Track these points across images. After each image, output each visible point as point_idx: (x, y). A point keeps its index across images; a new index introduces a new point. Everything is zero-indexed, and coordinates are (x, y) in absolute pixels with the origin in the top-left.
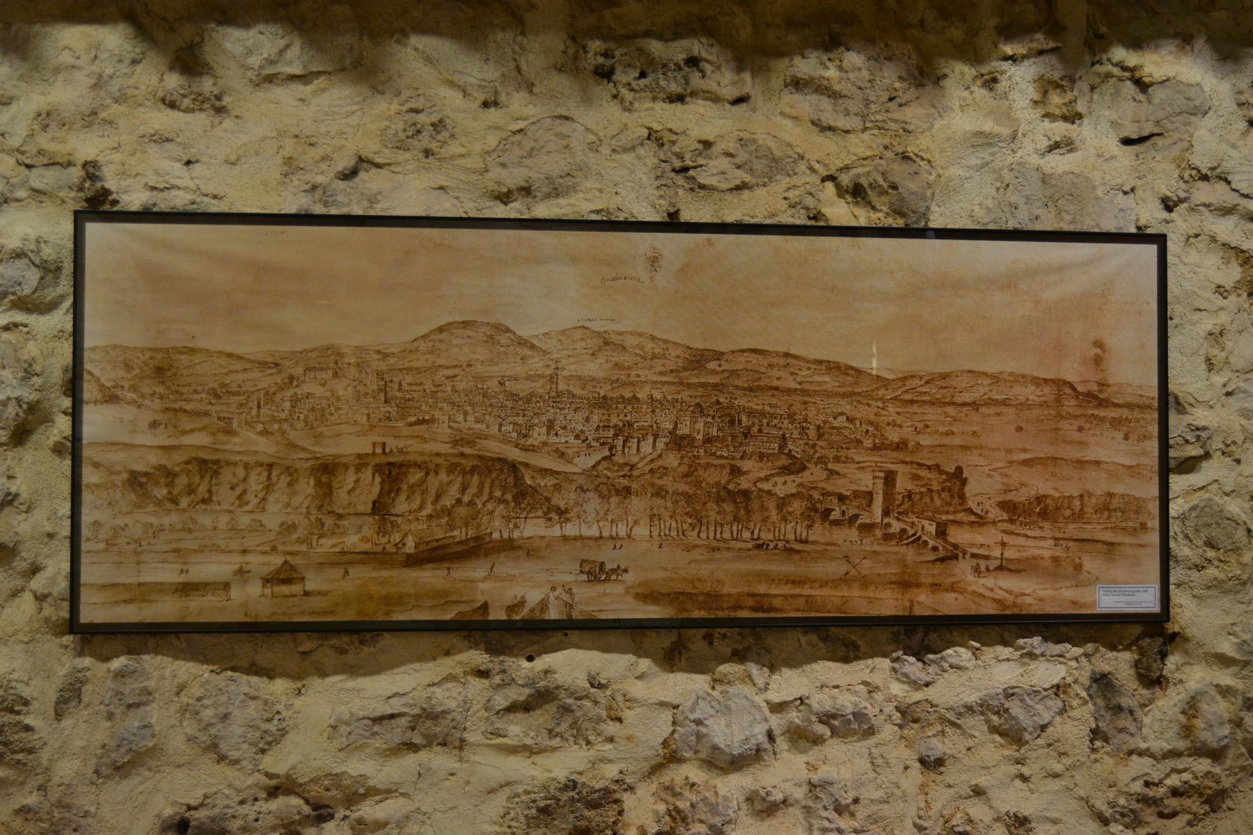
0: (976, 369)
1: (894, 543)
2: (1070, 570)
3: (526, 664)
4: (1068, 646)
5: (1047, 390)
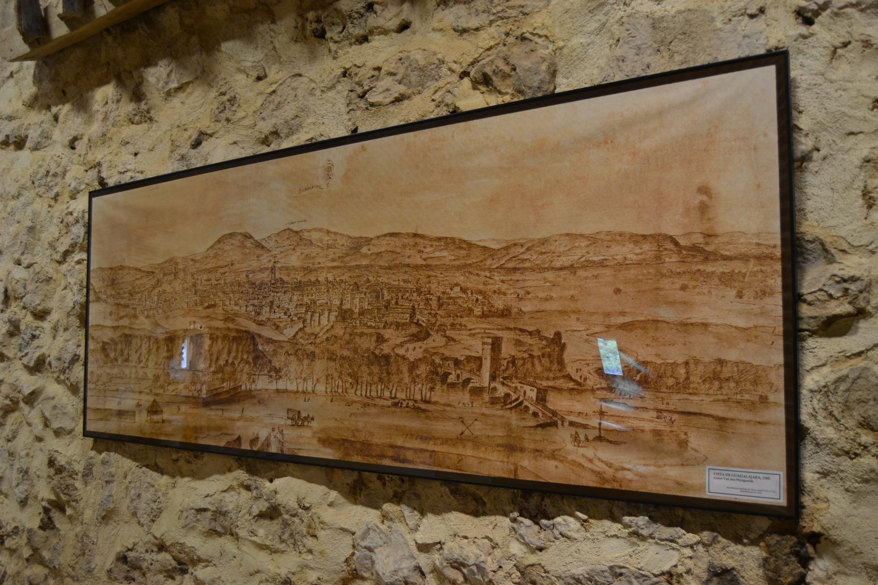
0: (574, 231)
1: (498, 407)
2: (674, 446)
3: (268, 484)
4: (680, 531)
5: (646, 247)
